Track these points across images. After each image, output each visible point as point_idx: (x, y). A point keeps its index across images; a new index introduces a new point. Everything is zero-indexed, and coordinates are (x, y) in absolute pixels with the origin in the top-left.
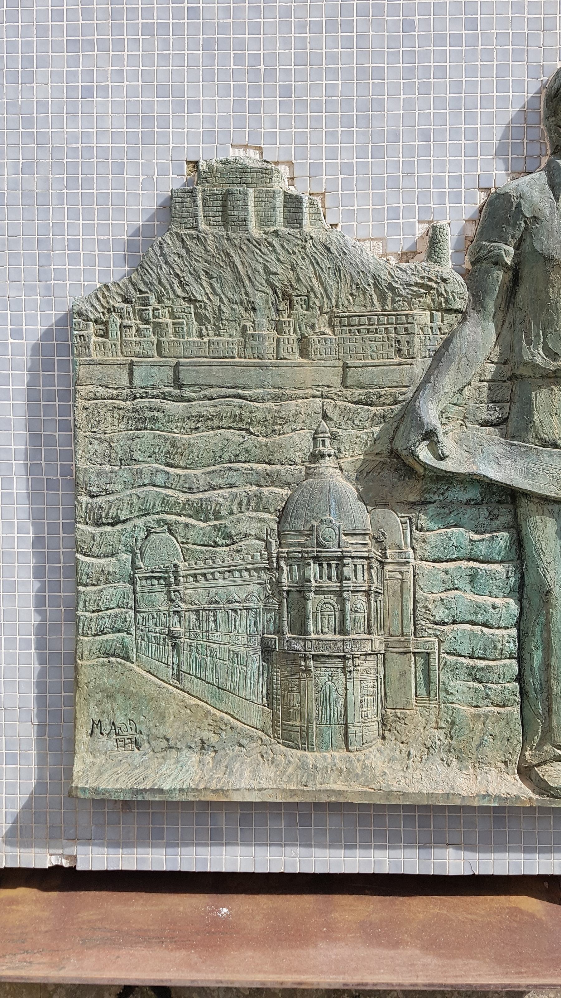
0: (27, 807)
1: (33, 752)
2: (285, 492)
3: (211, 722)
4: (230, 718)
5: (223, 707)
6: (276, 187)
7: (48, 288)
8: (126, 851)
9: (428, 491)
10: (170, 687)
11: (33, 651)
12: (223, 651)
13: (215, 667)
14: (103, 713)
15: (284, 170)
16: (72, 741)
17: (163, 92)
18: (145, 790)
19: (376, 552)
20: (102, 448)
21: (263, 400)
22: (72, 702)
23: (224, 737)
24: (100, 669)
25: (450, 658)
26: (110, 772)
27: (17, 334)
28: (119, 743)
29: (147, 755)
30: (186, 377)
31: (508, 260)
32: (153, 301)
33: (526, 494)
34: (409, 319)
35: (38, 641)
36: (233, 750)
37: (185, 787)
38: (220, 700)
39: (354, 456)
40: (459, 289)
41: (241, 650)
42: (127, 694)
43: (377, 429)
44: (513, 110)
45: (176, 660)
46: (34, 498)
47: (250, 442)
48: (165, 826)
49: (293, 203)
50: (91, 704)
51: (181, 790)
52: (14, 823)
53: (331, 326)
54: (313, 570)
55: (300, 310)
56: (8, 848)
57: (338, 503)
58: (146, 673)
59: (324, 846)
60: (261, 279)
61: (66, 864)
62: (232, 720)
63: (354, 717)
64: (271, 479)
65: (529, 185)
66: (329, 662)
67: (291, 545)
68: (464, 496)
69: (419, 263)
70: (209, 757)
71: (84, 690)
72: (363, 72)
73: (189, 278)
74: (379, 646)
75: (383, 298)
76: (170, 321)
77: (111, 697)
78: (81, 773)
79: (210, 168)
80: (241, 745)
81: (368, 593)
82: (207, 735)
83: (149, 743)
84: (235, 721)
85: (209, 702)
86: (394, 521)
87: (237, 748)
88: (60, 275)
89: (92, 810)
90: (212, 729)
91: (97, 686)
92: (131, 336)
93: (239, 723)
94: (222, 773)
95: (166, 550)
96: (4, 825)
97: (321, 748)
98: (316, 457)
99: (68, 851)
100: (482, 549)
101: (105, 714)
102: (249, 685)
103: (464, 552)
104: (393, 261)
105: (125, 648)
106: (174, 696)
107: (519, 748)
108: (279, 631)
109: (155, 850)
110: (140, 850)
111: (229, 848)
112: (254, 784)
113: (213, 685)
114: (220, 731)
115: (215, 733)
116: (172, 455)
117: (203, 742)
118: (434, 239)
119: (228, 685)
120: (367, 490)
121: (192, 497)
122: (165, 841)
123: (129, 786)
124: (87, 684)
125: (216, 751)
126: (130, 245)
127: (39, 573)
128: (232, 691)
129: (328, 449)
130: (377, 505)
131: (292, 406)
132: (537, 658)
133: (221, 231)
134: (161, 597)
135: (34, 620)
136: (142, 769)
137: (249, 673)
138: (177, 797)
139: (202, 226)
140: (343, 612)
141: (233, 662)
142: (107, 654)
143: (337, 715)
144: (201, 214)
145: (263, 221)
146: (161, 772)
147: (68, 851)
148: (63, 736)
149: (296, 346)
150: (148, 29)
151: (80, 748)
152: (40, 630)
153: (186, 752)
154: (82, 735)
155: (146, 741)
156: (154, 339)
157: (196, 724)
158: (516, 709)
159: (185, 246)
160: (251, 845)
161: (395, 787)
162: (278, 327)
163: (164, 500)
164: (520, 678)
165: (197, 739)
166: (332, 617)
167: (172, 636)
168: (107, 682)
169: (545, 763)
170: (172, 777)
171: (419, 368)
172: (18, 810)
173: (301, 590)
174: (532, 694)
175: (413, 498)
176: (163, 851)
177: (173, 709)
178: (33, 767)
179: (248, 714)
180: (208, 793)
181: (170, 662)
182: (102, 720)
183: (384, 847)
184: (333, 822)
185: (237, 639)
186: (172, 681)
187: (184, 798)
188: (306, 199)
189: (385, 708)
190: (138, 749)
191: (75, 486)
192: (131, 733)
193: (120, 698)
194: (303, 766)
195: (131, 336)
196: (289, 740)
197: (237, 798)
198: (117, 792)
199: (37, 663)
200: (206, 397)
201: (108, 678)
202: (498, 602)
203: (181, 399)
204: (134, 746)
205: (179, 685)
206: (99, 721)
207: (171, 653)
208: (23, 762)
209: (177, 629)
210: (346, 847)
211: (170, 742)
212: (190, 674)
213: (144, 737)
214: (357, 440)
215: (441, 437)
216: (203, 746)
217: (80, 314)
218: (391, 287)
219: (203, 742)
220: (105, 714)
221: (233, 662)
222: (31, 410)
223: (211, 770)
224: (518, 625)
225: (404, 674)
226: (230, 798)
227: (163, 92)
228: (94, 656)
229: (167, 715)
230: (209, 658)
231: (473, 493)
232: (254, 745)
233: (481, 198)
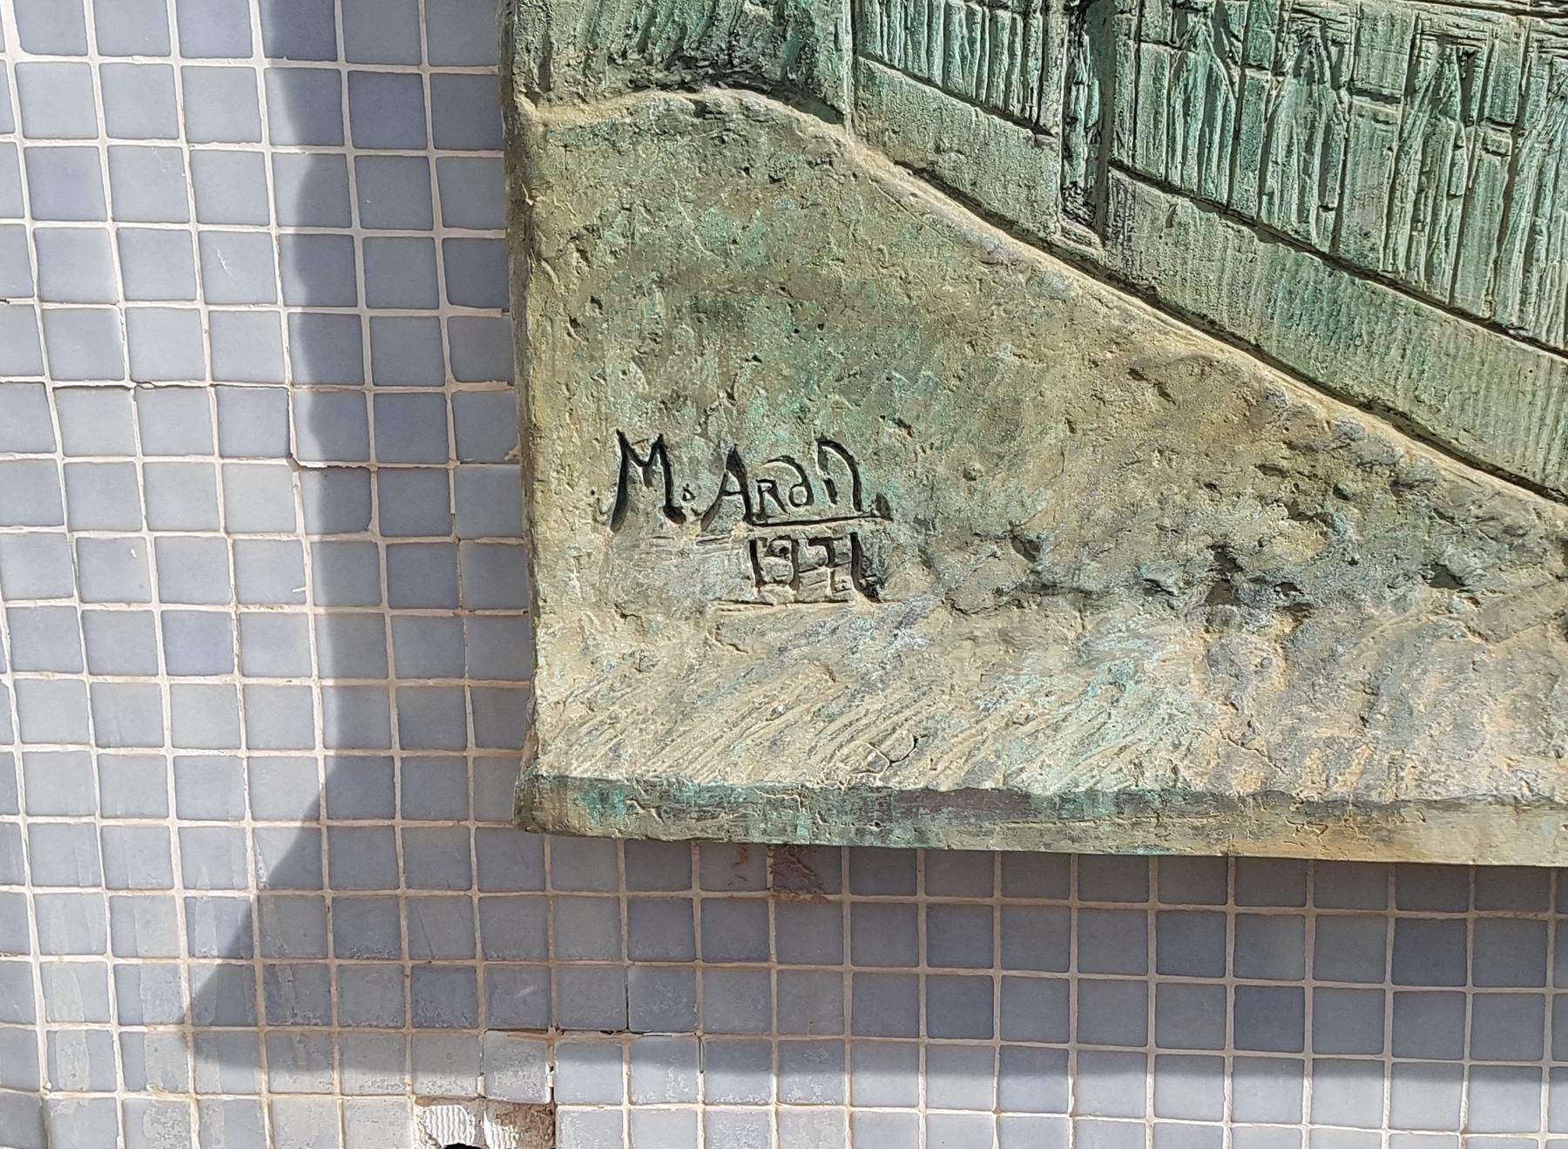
0: (295, 874)
1: (308, 609)
3: (1281, 456)
4: (1387, 431)
5: (1355, 374)
8: (798, 1084)
10: (1050, 265)
11: (260, 62)
13: (1325, 147)
14: (672, 403)
16: (515, 559)
18: (929, 798)
22: (508, 355)
23: (1352, 533)
24: (650, 154)
26: (730, 705)
28: (766, 561)
29: (920, 628)
36: (1401, 604)
37: (1148, 783)
38: (1338, 330)
42: (811, 302)
45: (1087, 101)
48: (997, 973)
50: (613, 352)
51: (1130, 800)
52: (233, 953)
56: (214, 1073)
62: (1401, 443)
70: (1260, 637)
71: (565, 280)
77: (719, 315)
78: (576, 711)
80: (1446, 578)
82: (1252, 522)
83: (928, 563)
84: (1420, 449)
85: (1271, 347)
87: (1422, 593)
89: (624, 894)
90: (1285, 490)
91: (636, 254)
93: (1444, 462)
94: (1348, 719)
96: (183, 963)
99: (511, 1084)
101: (690, 410)
102: (1519, 244)
106: (1071, 313)
109: (946, 1085)
110: (872, 1083)
111: (1334, 1089)
113: (1303, 245)
114: (1331, 505)
115: (1296, 514)
117: (1224, 555)
119: (1397, 248)
122: (997, 1042)
123: (843, 775)
124: (584, 241)
125: (1299, 611)
128: (1418, 277)
136: (899, 690)
137: (1529, 173)
138: (1105, 836)
141: (1439, 106)
142: (689, 63)
146: (1004, 708)
147: (511, 1084)
148: (458, 530)
151: (562, 588)
153: (1127, 612)
154: (570, 519)
155: (912, 554)
157: (1189, 467)
160: (1455, 1074)
165: (1196, 548)
168: (697, 226)
170: (1071, 733)
172: (252, 894)
176: (986, 1088)
177: (1066, 382)
178: (312, 682)
179: (1499, 409)
180: (1281, 817)
181: (1052, 116)
182: (671, 438)
186: (1056, 225)
190: (871, 594)
192: (831, 510)
193: (768, 322)
198: (777, 805)
199: (286, 130)
201: (699, 204)
204: (844, 576)
205: (1097, 252)
206: (660, 446)
207: (1060, 55)
208: (256, 659)
211: (1046, 559)
212: (1166, 186)
213: (902, 532)
216: (1228, 579)
219: (1224, 555)
220: (690, 410)
221: (1439, 106)
223: (1285, 702)
226: (1408, 846)
228: (613, 78)
229: (1028, 416)
230: (1290, 83)
232: (1524, 577)
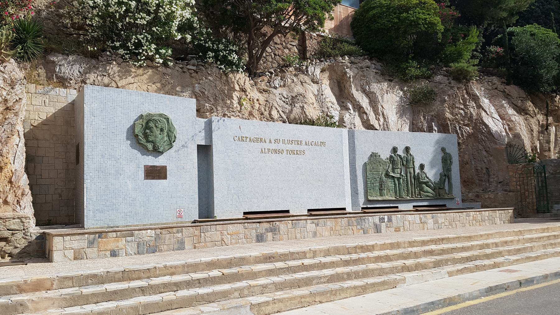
214: (384, 172)
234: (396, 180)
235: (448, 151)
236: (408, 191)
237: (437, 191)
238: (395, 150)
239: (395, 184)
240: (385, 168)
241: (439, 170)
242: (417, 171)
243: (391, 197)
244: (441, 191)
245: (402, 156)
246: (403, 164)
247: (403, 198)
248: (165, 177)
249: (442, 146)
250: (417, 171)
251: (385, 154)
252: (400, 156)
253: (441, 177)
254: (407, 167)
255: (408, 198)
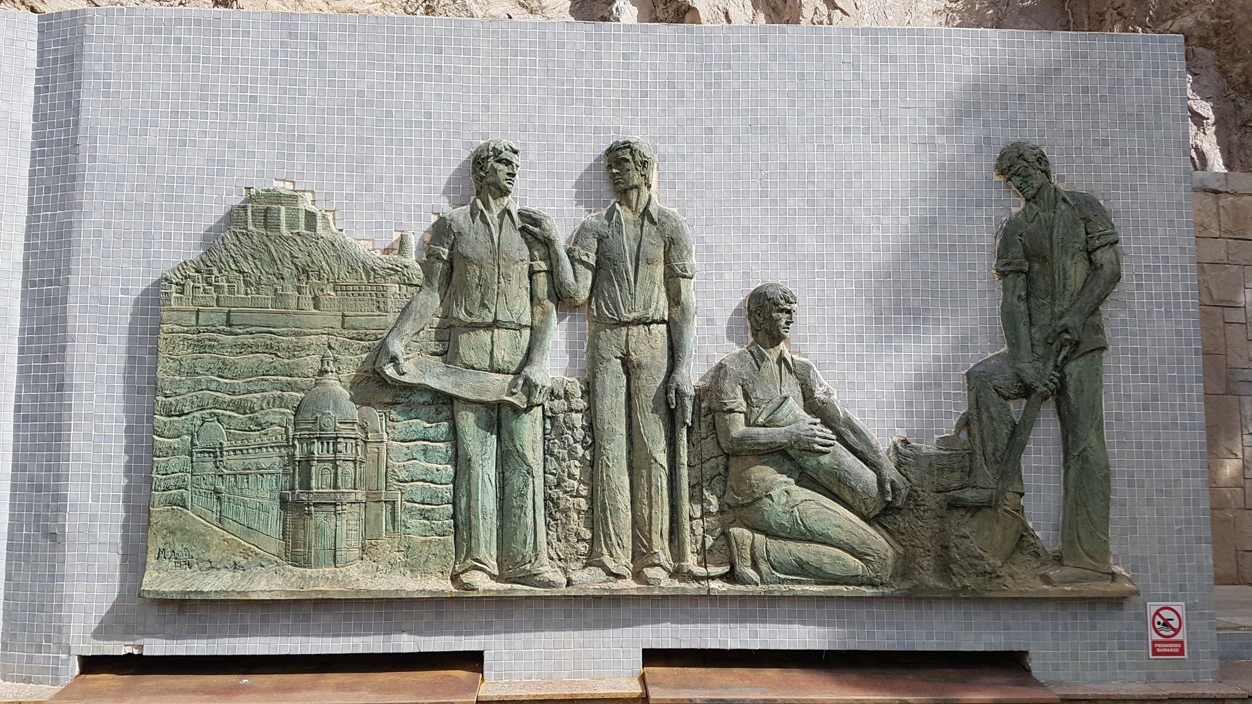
2: (300, 395)
6: (301, 206)
7: (149, 262)
9: (397, 396)
12: (252, 502)
15: (308, 196)
17: (232, 145)
19: (360, 434)
20: (175, 365)
21: (287, 335)
25: (408, 504)
27: (125, 291)
30: (234, 320)
31: (445, 257)
32: (215, 271)
33: (457, 398)
34: (385, 289)
35: (125, 497)
38: (249, 536)
39: (349, 373)
40: (417, 273)
41: (265, 502)
42: (184, 531)
43: (365, 356)
44: (453, 168)
46: (128, 399)
47: (277, 362)
49: (311, 216)
53: (336, 291)
54: (317, 447)
55: (314, 280)
57: (335, 403)
58: (199, 515)
59: (318, 636)
60: (288, 261)
61: (136, 652)
63: (342, 544)
64: (291, 387)
65: (458, 214)
66: (325, 508)
67: (302, 430)
68: (421, 400)
69: (394, 256)
70: (239, 574)
72: (360, 140)
73: (240, 258)
74: (361, 496)
75: (368, 276)
76: (226, 284)
77: (173, 533)
79: (258, 193)
81: (354, 461)
86: (376, 416)
88: (158, 255)
92: (200, 293)
95: (218, 433)
97: (317, 566)
98: (323, 372)
100: (431, 433)
103: (420, 435)
104: (379, 254)
105: (183, 499)
107: (452, 563)
108: (292, 489)
112: (267, 588)
116: (223, 369)
118: (402, 242)
119: (255, 526)
120: (357, 394)
121: (234, 398)
126: (205, 237)
127: (128, 450)
129: (332, 367)
130: (363, 404)
131: (307, 339)
132: (464, 501)
133: (263, 231)
134: (210, 465)
135: (124, 482)
139: (251, 227)
140: (336, 474)
143: (328, 543)
144: (250, 221)
145: (291, 226)
147: (137, 642)
149: (311, 302)
150: (224, 107)
152: (127, 489)
153: (223, 571)
154: (151, 559)
156: (215, 295)
158: (451, 538)
159: (238, 239)
161: (363, 587)
162: (299, 290)
163: (215, 399)
164: (454, 517)
166: (329, 478)
167: (216, 491)
169: (466, 571)
171: (391, 319)
173: (308, 460)
174: (461, 527)
175: (387, 400)
183: (360, 635)
184: (326, 618)
185: (264, 493)
187: (217, 597)
188: (319, 215)
189: (364, 539)
191: (156, 389)
193: (179, 534)
194: (303, 577)
195: (200, 293)
196: (296, 562)
197: (254, 597)
200: (247, 333)
202: (440, 467)
203: (231, 334)
209: (221, 487)
210: (334, 636)
214: (351, 362)
215: (401, 361)
217: (166, 280)
218: (374, 270)
222: (130, 340)
224: (454, 482)
225: (378, 516)
227: (232, 145)
231: (427, 398)
233: (434, 219)
234: (468, 421)
235: (1068, 176)
236: (596, 515)
237: (924, 529)
238: (486, 174)
239: (460, 460)
240: (365, 315)
241: (963, 344)
242: (711, 345)
243: (413, 567)
244: (965, 528)
245: (561, 235)
246: (560, 296)
247: (529, 579)
248: (644, 650)
249: (1005, 136)
250: (711, 345)
251: (382, 209)
252: (533, 230)
253: (977, 404)
254: (602, 315)
255: (589, 581)
